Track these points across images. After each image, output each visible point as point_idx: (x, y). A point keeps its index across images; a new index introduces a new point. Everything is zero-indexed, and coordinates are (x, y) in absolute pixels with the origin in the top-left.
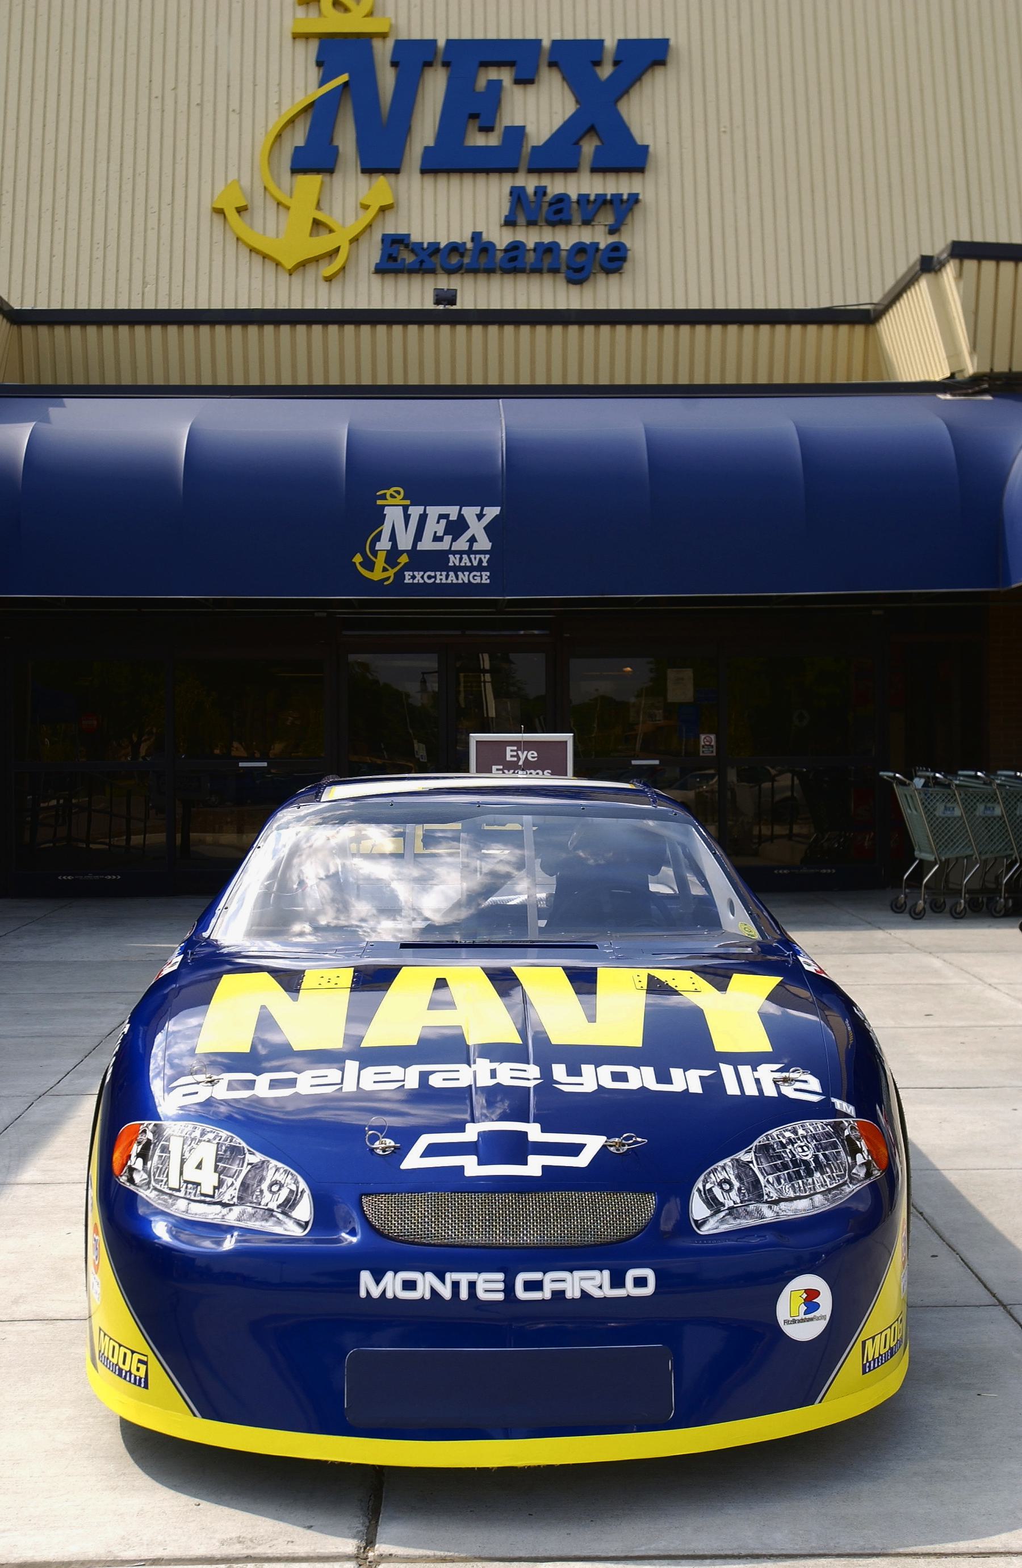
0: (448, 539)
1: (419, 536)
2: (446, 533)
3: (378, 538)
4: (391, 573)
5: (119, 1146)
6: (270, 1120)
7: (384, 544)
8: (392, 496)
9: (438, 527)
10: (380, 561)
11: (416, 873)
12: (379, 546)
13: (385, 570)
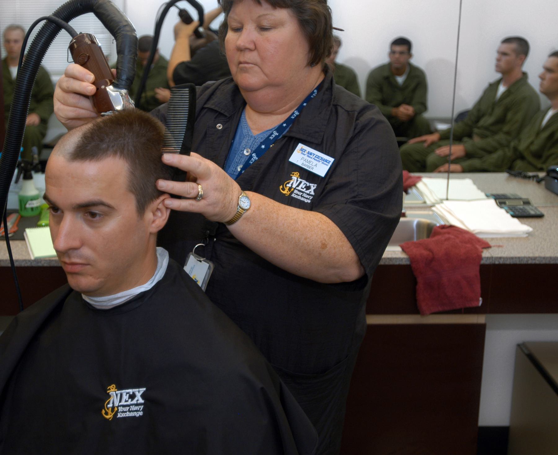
0: (130, 400)
1: (298, 186)
2: (305, 187)
3: (288, 183)
4: (289, 193)
5: (112, 305)
6: (5, 208)
7: (289, 185)
8: (112, 389)
9: (125, 397)
10: (287, 189)
11: (527, 208)
12: (288, 185)
13: (287, 192)
